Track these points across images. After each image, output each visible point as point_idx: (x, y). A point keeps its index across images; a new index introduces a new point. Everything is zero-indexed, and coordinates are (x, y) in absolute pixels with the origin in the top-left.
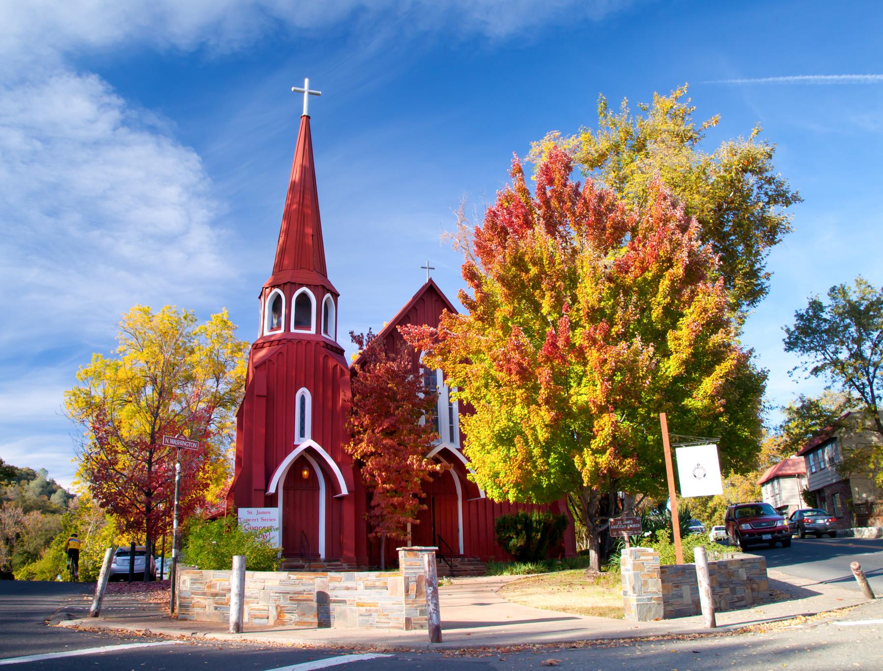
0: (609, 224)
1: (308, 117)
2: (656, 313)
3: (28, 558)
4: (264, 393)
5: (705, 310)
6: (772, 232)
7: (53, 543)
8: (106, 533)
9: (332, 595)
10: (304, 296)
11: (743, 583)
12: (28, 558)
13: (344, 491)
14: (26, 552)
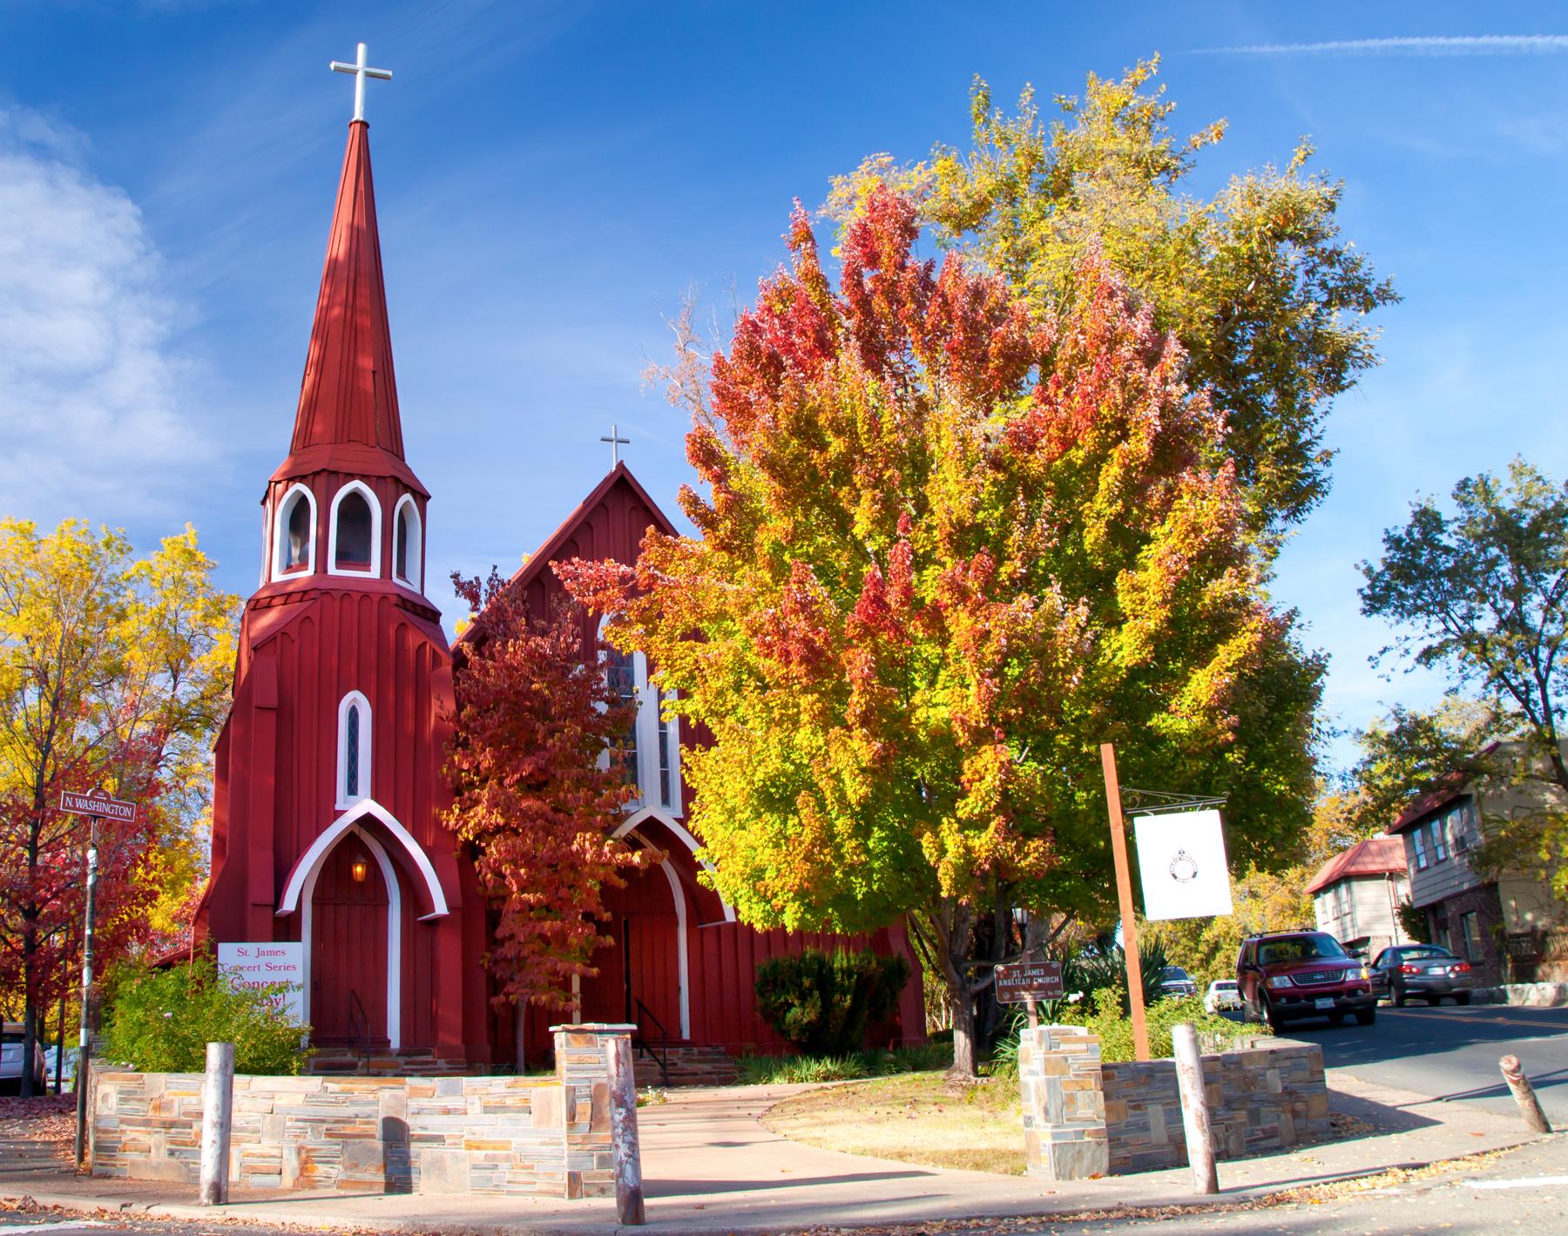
5: (1196, 529)
6: (1335, 367)
9: (415, 1125)
10: (355, 499)
11: (1275, 1101)
13: (441, 907)
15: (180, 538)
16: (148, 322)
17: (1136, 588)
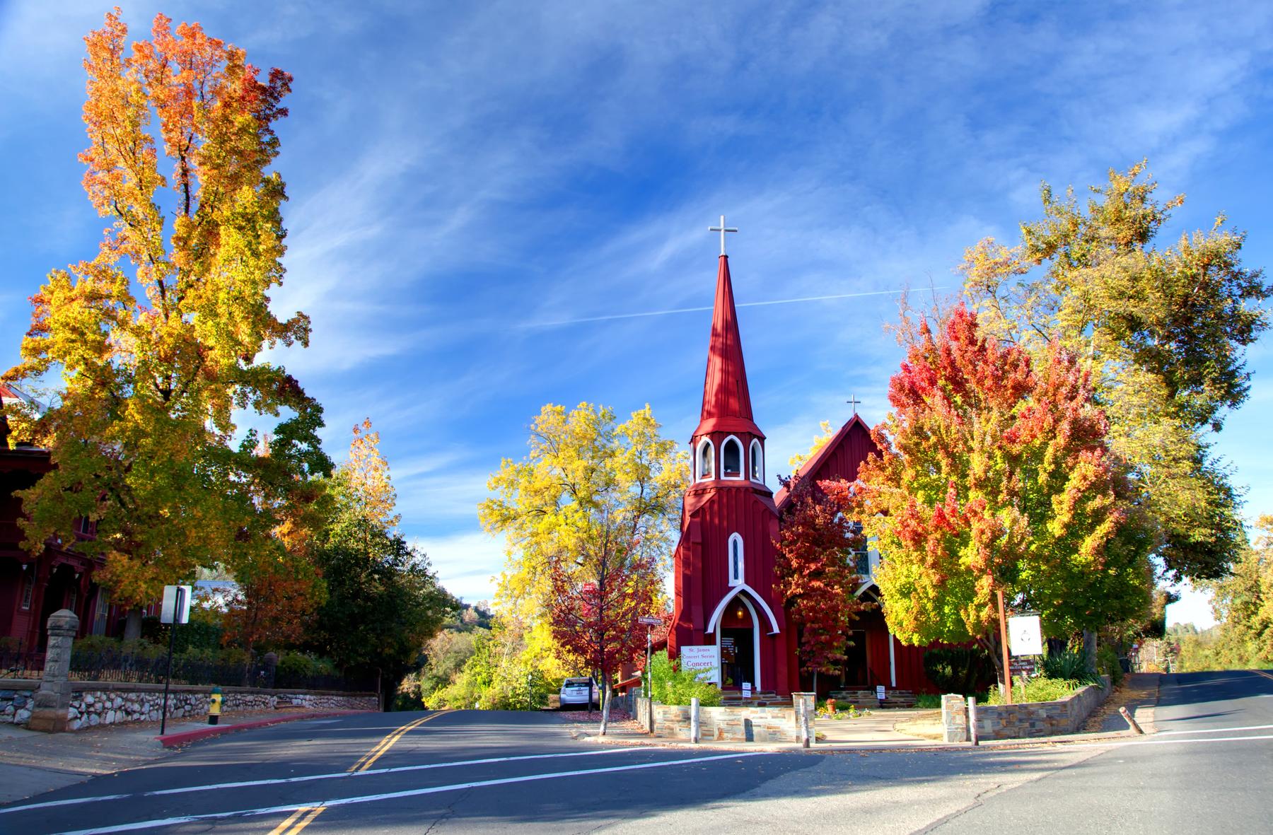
0: (1010, 384)
1: (726, 257)
2: (1042, 478)
3: (437, 684)
4: (699, 540)
5: (1085, 478)
6: (1245, 329)
7: (465, 667)
8: (527, 656)
9: (754, 722)
10: (732, 442)
11: (1043, 720)
12: (437, 684)
13: (776, 630)
14: (435, 676)
17: (1061, 503)
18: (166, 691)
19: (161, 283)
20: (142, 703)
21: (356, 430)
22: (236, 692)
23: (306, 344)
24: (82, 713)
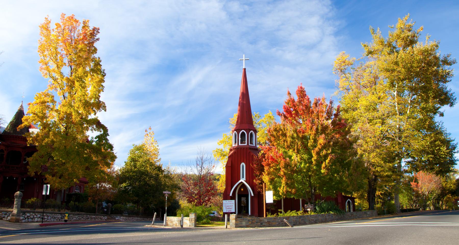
1: (245, 69)
6: (444, 78)
10: (243, 132)
11: (266, 222)
15: (268, 114)
16: (331, 28)
18: (43, 213)
19: (64, 96)
20: (48, 216)
21: (146, 131)
22: (79, 215)
23: (105, 111)
24: (26, 218)
